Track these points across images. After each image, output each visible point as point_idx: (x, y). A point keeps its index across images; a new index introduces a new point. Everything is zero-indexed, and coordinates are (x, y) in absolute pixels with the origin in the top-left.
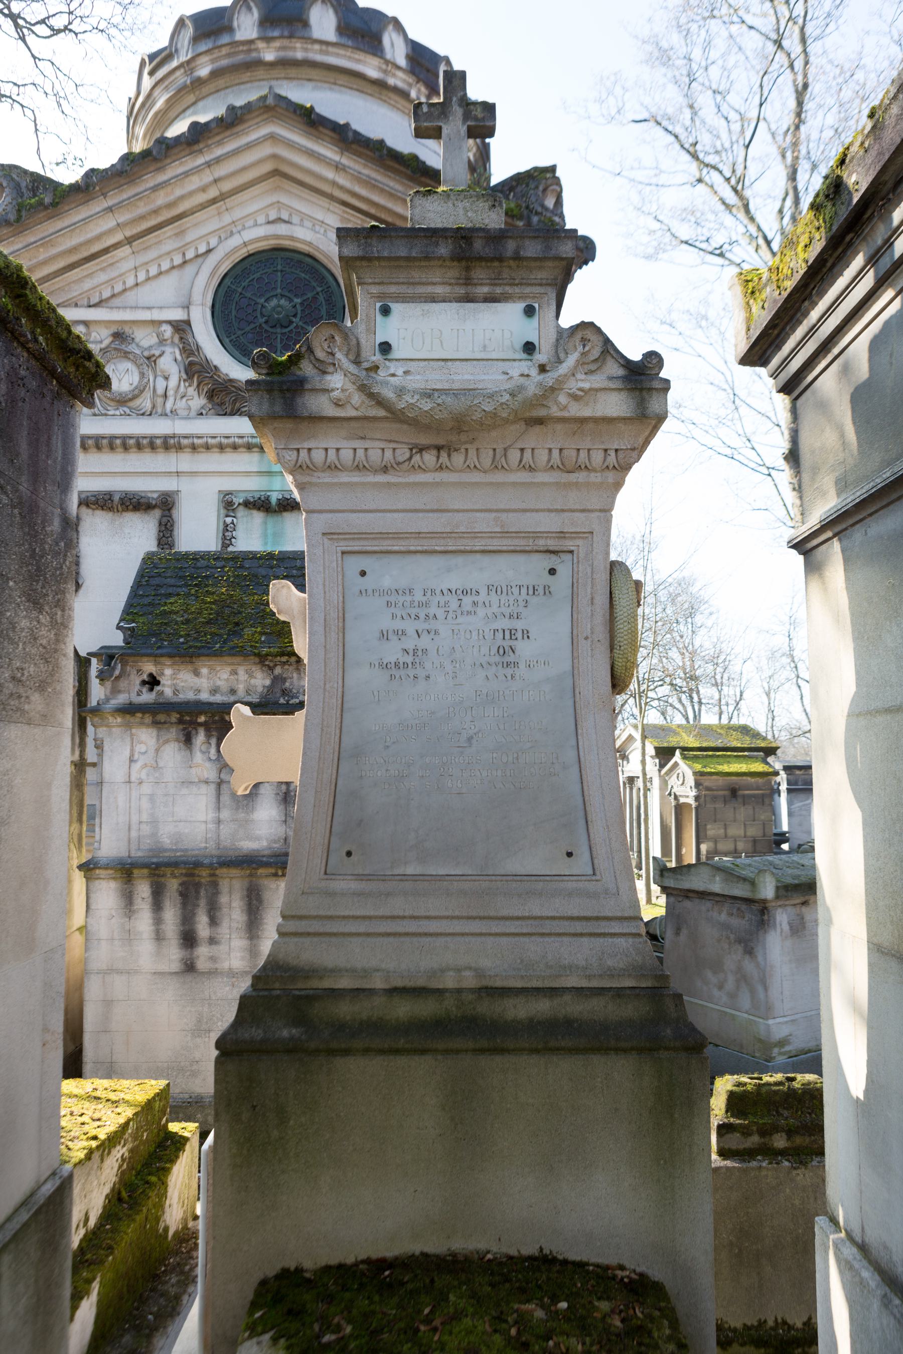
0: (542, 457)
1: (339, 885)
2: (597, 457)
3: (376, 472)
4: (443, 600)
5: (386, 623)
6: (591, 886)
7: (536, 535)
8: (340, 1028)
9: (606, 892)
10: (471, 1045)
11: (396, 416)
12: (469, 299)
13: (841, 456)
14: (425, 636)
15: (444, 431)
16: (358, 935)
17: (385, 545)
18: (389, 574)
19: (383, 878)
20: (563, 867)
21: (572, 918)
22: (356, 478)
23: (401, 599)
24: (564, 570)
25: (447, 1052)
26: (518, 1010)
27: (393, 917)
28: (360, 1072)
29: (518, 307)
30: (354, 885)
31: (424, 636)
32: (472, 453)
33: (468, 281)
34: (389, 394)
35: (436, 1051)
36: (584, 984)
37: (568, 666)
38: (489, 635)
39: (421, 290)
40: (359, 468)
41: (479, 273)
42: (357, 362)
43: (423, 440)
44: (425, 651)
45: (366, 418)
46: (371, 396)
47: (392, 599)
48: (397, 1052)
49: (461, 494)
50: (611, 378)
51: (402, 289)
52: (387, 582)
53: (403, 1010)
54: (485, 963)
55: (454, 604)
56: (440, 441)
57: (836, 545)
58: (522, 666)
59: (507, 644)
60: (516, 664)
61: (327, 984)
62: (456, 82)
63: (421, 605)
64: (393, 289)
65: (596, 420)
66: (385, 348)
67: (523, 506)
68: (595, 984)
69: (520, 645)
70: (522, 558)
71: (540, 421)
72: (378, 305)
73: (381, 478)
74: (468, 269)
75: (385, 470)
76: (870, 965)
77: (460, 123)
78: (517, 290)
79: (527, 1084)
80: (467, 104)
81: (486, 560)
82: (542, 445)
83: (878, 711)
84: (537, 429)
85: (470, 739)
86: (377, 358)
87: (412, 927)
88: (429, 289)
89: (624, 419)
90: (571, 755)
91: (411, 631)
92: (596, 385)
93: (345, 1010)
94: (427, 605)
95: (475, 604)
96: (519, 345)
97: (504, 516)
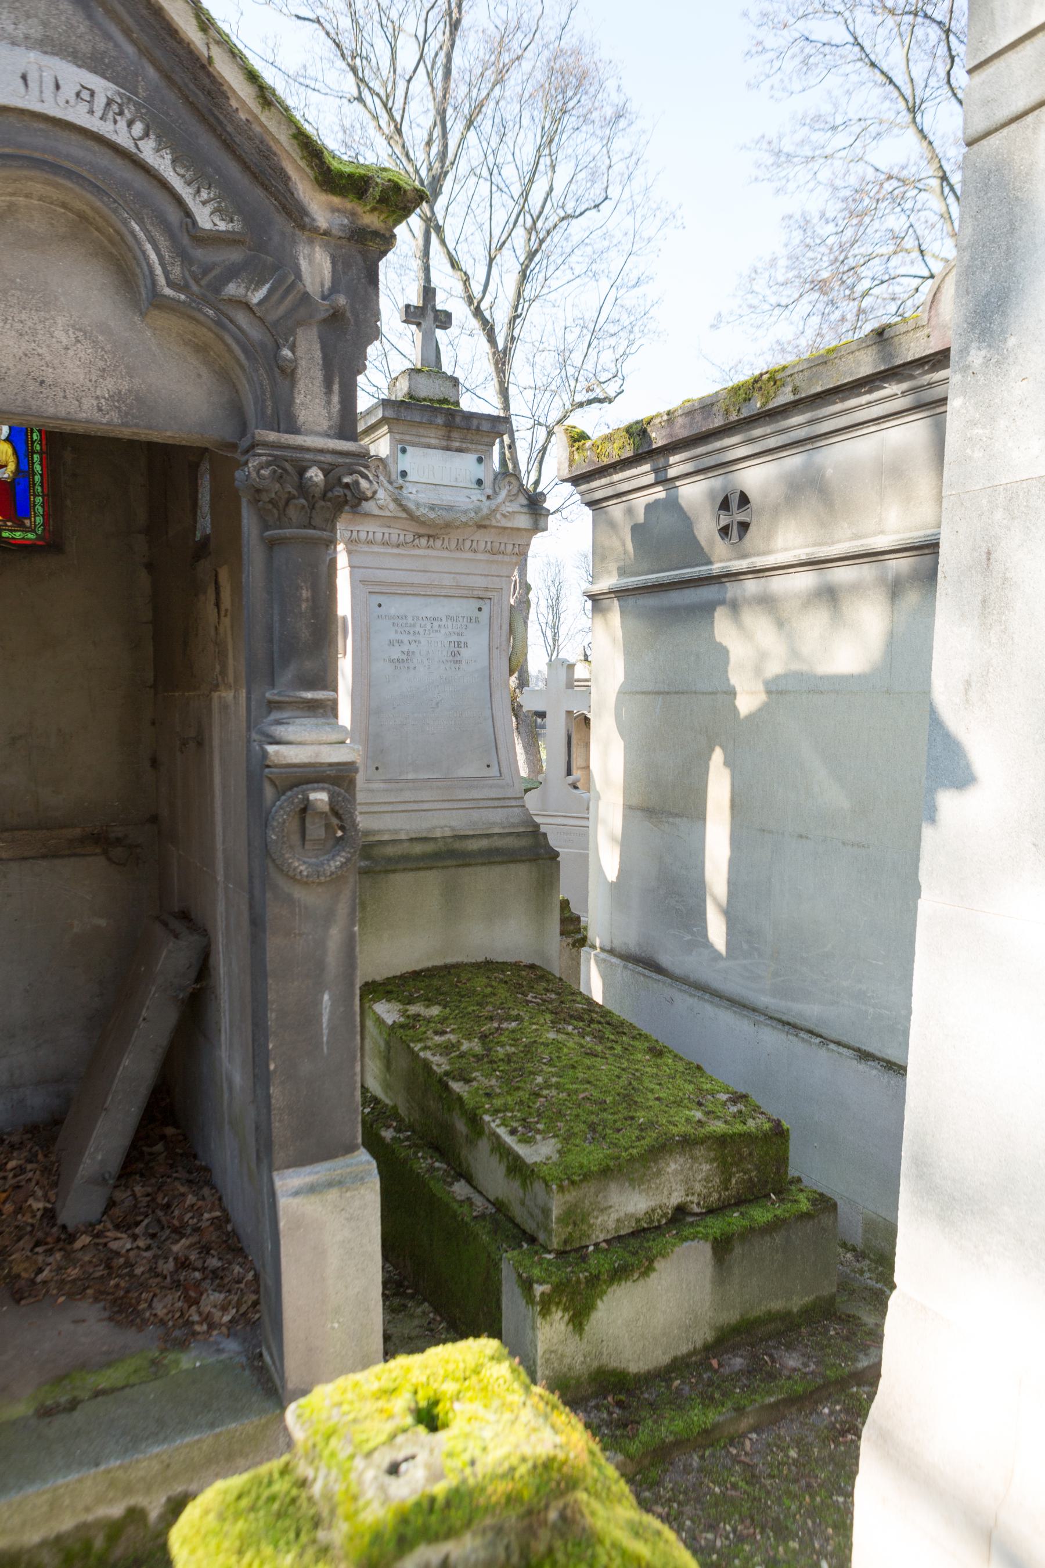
0: (482, 545)
1: (375, 786)
2: (510, 547)
3: (393, 546)
4: (423, 623)
5: (393, 636)
6: (500, 782)
7: (473, 589)
8: (389, 860)
9: (508, 785)
10: (455, 863)
11: (411, 516)
12: (448, 449)
13: (622, 556)
14: (414, 645)
15: (431, 528)
16: (387, 812)
17: (393, 590)
18: (395, 607)
19: (397, 781)
20: (486, 773)
21: (492, 799)
22: (382, 549)
23: (401, 621)
24: (486, 609)
25: (443, 867)
26: (473, 845)
27: (405, 802)
28: (402, 881)
29: (473, 457)
30: (382, 786)
31: (413, 644)
32: (446, 541)
33: (449, 438)
34: (412, 506)
35: (437, 867)
36: (502, 831)
37: (487, 664)
38: (447, 645)
39: (423, 440)
40: (385, 544)
41: (455, 435)
42: (391, 483)
43: (421, 531)
44: (413, 653)
45: (395, 517)
46: (400, 505)
47: (396, 621)
48: (419, 869)
49: (437, 563)
50: (522, 506)
51: (413, 438)
52: (393, 612)
53: (418, 849)
54: (453, 823)
55: (429, 626)
56: (431, 533)
57: (616, 602)
58: (464, 662)
59: (456, 650)
60: (460, 662)
61: (377, 838)
62: (430, 295)
63: (411, 626)
64: (407, 438)
65: (512, 529)
66: (404, 474)
67: (467, 571)
68: (506, 831)
69: (463, 651)
70: (464, 601)
71: (485, 527)
72: (400, 446)
73: (395, 551)
74: (450, 432)
75: (398, 546)
76: (624, 815)
77: (432, 322)
78: (474, 446)
79: (481, 880)
80: (436, 312)
81: (446, 601)
82: (483, 538)
83: (637, 693)
84: (482, 530)
85: (437, 704)
86: (400, 481)
87: (415, 807)
88: (428, 440)
89: (525, 530)
90: (489, 712)
91: (406, 641)
92: (515, 510)
93: (390, 851)
94: (414, 626)
95: (440, 626)
96: (474, 480)
97: (458, 577)
